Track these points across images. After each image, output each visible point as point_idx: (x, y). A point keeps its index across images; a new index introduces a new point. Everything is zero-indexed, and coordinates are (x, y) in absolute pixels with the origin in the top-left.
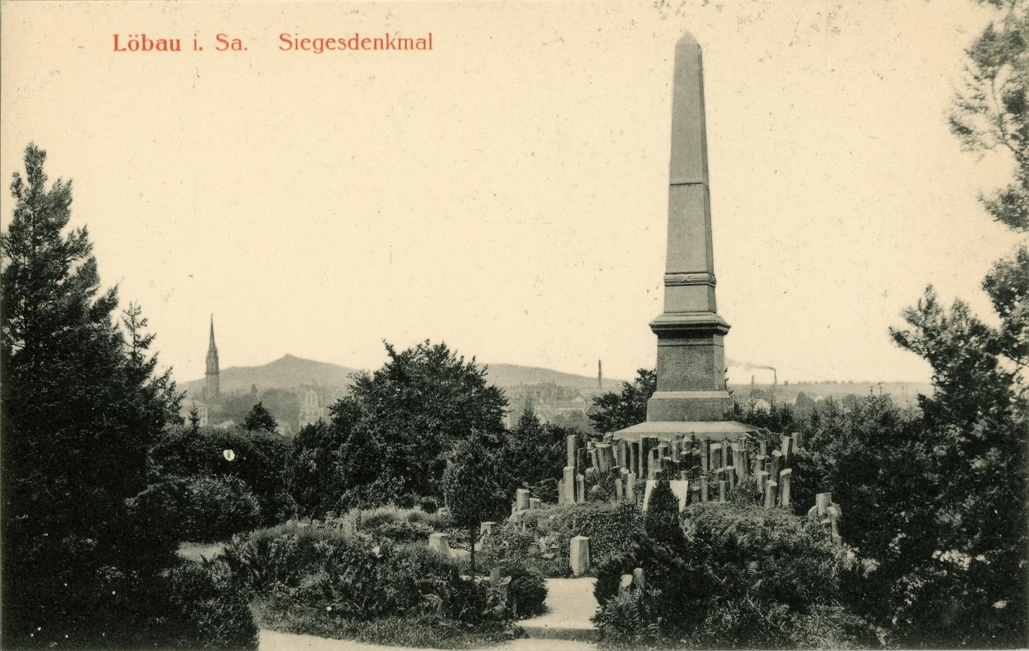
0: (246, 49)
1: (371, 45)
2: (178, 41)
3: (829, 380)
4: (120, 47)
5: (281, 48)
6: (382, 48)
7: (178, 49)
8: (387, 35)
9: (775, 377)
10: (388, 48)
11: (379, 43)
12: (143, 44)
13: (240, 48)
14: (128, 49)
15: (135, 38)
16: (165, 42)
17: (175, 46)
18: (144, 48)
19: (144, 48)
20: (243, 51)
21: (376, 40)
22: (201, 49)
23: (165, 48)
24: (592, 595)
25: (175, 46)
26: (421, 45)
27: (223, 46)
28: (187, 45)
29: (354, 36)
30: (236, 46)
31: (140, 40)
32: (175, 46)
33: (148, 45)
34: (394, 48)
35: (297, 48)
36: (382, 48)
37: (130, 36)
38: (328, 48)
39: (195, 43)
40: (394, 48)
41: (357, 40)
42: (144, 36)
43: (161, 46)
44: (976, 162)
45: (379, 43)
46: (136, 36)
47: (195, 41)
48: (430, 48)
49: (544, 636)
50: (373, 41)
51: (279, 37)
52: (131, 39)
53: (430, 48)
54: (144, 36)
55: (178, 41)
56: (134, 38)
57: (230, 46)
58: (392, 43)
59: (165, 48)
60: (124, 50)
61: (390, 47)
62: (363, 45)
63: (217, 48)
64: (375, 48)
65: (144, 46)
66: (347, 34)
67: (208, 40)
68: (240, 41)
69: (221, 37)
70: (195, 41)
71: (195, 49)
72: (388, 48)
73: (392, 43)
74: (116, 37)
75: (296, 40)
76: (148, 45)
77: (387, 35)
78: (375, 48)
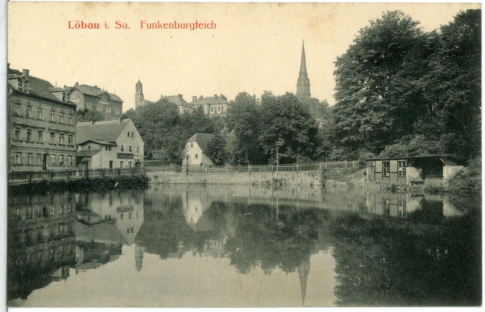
1: (168, 26)
2: (98, 24)
3: (142, 268)
4: (71, 27)
6: (156, 28)
7: (98, 27)
8: (159, 22)
9: (303, 48)
10: (159, 28)
11: (171, 26)
12: (82, 25)
13: (126, 28)
17: (97, 26)
19: (82, 27)
21: (170, 24)
24: (164, 261)
27: (119, 26)
28: (102, 26)
31: (80, 23)
32: (97, 26)
34: (161, 27)
36: (156, 28)
38: (200, 28)
39: (106, 25)
42: (82, 22)
43: (90, 26)
45: (171, 26)
46: (79, 21)
48: (215, 28)
49: (304, 51)
52: (76, 23)
53: (215, 28)
54: (82, 22)
55: (98, 24)
56: (77, 22)
57: (122, 26)
58: (161, 25)
59: (92, 28)
60: (73, 28)
61: (160, 27)
62: (199, 26)
63: (116, 28)
64: (170, 28)
65: (181, 27)
67: (112, 25)
68: (126, 24)
69: (118, 22)
71: (106, 28)
72: (159, 28)
75: (205, 24)
77: (159, 22)
78: (170, 28)
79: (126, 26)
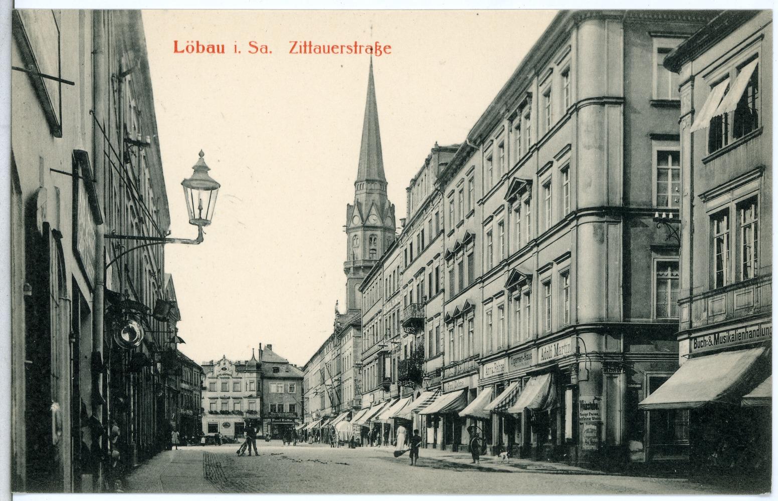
4: (179, 49)
7: (223, 52)
13: (266, 52)
14: (185, 51)
15: (192, 44)
18: (198, 51)
19: (198, 51)
22: (240, 52)
23: (213, 51)
26: (317, 51)
28: (229, 49)
30: (264, 50)
33: (201, 48)
37: (188, 42)
42: (198, 42)
43: (211, 50)
47: (235, 46)
51: (248, 44)
56: (190, 43)
59: (213, 51)
67: (244, 47)
69: (253, 44)
76: (201, 48)
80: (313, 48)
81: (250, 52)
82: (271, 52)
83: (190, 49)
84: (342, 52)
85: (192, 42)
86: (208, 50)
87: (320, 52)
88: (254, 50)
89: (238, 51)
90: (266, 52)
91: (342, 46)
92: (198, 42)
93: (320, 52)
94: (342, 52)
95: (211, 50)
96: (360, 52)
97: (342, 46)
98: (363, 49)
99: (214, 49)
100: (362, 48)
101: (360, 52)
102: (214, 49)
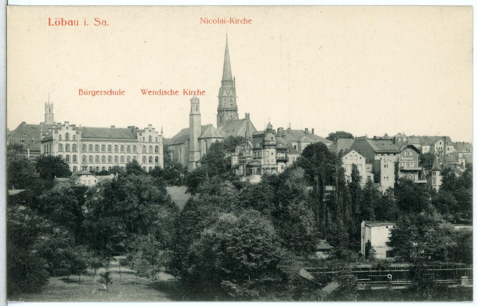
0: (88, 25)
4: (51, 24)
5: (95, 25)
13: (106, 25)
15: (59, 20)
16: (72, 22)
18: (62, 25)
19: (62, 25)
20: (107, 26)
21: (153, 91)
22: (88, 25)
23: (72, 24)
25: (76, 23)
26: (222, 22)
28: (81, 23)
29: (110, 91)
30: (104, 24)
33: (64, 23)
34: (187, 94)
35: (207, 23)
37: (56, 19)
40: (187, 94)
41: (160, 91)
42: (62, 19)
43: (70, 23)
44: (184, 90)
47: (85, 21)
50: (152, 92)
51: (94, 20)
52: (56, 20)
55: (78, 21)
56: (57, 20)
58: (186, 92)
59: (72, 24)
60: (53, 25)
66: (157, 90)
69: (97, 19)
70: (85, 21)
73: (186, 92)
74: (50, 19)
76: (64, 23)
79: (105, 23)
80: (219, 21)
81: (95, 25)
82: (108, 25)
83: (58, 23)
84: (101, 94)
85: (59, 19)
86: (68, 23)
87: (223, 23)
88: (98, 23)
89: (86, 24)
90: (106, 25)
91: (101, 91)
92: (62, 19)
93: (223, 23)
94: (101, 94)
95: (70, 23)
96: (238, 23)
97: (101, 91)
98: (239, 21)
99: (71, 23)
100: (239, 21)
101: (238, 23)
102: (71, 23)
